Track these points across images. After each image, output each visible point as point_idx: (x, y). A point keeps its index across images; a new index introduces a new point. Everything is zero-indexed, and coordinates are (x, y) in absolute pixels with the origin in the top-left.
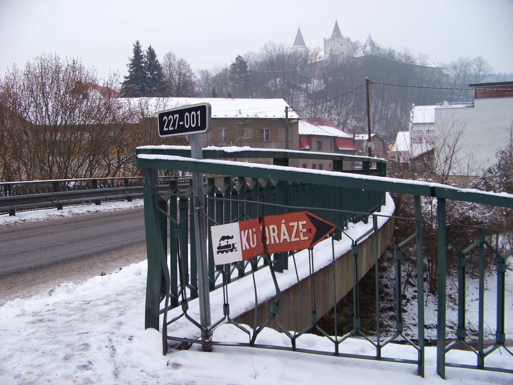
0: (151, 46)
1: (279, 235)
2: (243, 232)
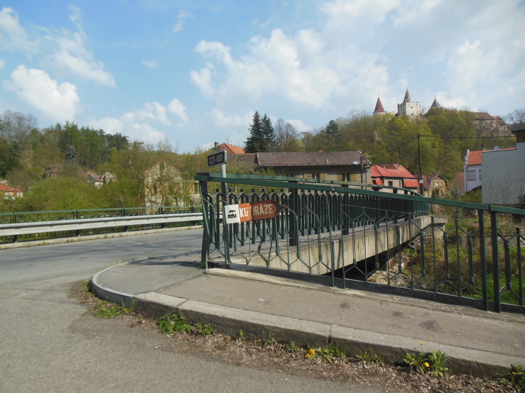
0: (265, 115)
1: (259, 211)
2: (240, 209)
